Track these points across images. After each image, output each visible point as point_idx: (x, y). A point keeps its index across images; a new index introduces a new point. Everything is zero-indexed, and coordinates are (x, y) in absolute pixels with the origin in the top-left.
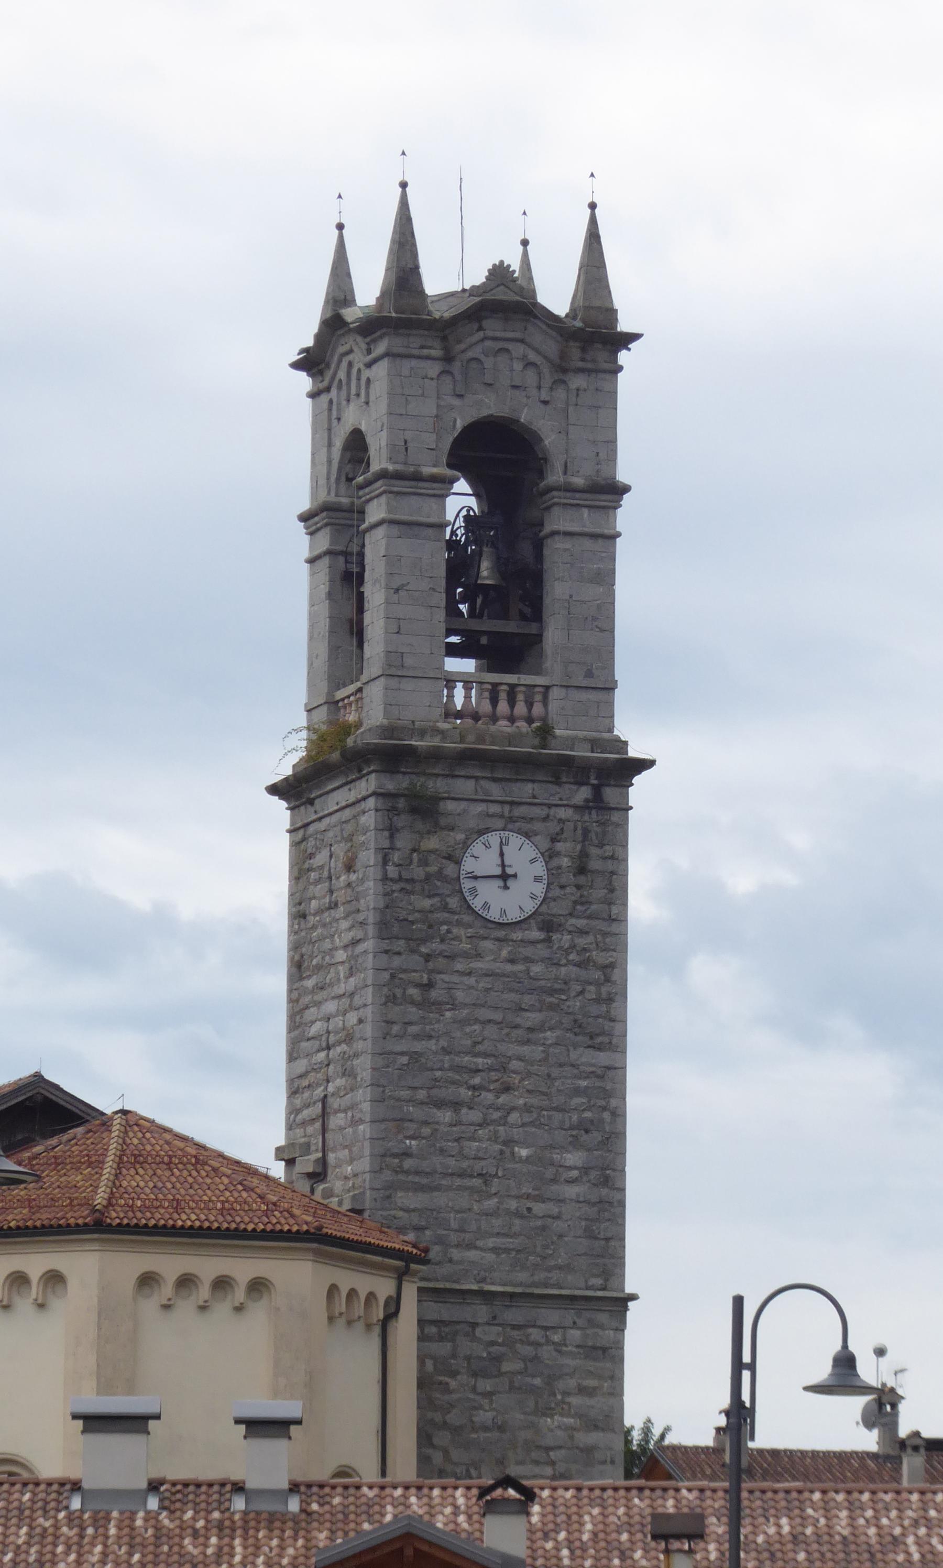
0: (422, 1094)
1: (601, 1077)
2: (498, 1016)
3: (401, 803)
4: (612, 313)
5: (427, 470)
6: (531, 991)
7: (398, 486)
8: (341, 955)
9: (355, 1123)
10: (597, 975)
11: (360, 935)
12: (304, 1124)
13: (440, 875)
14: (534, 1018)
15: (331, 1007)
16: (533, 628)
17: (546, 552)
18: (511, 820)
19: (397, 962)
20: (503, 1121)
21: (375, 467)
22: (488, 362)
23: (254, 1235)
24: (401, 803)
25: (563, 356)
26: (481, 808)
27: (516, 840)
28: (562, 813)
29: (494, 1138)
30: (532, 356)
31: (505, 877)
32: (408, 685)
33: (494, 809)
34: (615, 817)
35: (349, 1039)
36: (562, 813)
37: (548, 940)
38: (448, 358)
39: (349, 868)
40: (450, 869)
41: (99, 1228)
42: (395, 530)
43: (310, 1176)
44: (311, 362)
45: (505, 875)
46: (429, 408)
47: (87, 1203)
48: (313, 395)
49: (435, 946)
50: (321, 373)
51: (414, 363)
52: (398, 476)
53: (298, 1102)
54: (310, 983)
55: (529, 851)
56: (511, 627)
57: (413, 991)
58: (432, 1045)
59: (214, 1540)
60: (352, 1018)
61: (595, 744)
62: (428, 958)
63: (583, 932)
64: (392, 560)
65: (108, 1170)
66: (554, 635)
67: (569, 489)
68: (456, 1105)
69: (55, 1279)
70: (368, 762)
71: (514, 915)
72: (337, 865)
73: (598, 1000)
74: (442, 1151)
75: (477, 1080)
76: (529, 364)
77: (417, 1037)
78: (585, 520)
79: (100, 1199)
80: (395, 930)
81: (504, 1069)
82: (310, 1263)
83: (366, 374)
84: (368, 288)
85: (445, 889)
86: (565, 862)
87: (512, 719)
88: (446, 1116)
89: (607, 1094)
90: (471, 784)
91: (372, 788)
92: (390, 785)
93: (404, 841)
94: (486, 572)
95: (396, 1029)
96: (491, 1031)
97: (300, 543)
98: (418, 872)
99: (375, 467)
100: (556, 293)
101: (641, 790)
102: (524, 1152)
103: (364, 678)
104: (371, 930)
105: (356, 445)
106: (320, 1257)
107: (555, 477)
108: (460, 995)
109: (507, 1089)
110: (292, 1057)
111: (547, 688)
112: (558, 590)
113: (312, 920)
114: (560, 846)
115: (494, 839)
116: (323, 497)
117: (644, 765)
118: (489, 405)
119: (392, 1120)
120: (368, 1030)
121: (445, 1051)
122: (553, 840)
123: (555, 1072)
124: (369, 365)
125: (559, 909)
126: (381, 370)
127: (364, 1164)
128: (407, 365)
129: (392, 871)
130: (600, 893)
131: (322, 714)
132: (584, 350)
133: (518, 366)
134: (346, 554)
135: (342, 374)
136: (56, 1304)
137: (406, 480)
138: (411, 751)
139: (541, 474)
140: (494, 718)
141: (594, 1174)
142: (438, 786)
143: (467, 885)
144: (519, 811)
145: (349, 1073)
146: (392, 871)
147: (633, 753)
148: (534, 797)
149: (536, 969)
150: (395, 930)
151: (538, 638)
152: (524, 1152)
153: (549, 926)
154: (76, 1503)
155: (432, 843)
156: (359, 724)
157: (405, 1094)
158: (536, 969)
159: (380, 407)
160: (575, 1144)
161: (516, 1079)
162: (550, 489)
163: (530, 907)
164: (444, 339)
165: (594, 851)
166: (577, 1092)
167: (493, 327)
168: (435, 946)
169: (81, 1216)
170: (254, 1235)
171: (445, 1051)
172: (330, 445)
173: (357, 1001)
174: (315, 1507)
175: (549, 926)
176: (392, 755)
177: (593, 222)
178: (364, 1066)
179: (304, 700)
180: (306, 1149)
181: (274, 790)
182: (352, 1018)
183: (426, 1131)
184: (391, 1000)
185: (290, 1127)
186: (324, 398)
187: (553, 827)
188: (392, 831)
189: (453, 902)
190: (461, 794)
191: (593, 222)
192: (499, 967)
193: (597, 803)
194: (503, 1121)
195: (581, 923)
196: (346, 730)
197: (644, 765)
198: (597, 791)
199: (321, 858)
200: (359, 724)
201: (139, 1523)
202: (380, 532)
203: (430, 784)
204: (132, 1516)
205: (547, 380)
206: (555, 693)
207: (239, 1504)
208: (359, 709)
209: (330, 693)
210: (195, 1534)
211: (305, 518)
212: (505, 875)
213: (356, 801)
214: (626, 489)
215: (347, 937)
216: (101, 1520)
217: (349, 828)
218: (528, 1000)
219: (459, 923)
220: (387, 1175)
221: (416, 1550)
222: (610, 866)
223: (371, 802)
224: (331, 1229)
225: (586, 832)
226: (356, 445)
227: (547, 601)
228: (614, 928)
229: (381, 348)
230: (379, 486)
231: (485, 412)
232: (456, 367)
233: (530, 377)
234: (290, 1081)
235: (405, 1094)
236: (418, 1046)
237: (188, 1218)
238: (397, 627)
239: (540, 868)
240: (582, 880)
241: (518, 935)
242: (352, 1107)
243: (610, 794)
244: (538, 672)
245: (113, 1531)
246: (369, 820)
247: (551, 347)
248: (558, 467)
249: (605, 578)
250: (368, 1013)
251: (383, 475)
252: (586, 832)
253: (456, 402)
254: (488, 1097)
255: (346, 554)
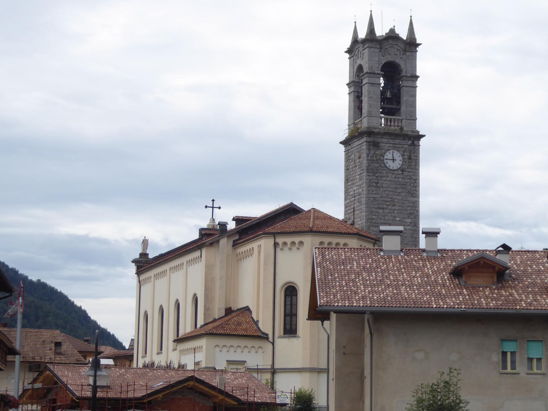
0: (376, 206)
1: (414, 203)
2: (392, 190)
3: (371, 144)
4: (415, 39)
5: (377, 72)
6: (399, 184)
7: (370, 75)
8: (358, 177)
9: (361, 212)
10: (413, 181)
11: (362, 172)
12: (349, 214)
13: (380, 159)
14: (400, 190)
15: (355, 188)
16: (398, 107)
17: (401, 90)
18: (395, 147)
19: (371, 178)
20: (393, 212)
21: (365, 71)
22: (389, 49)
23: (345, 234)
24: (371, 144)
25: (405, 48)
26: (388, 145)
27: (396, 152)
28: (406, 146)
29: (391, 216)
30: (398, 48)
31: (393, 160)
32: (372, 118)
33: (391, 145)
34: (417, 147)
35: (360, 194)
36: (406, 146)
37: (403, 174)
38: (381, 48)
39: (359, 158)
40: (382, 158)
41: (311, 232)
42: (370, 85)
43: (351, 224)
44: (350, 51)
45: (394, 159)
46: (377, 59)
47: (308, 226)
48: (349, 58)
49: (379, 174)
50: (352, 53)
51: (373, 49)
52: (370, 73)
53: (347, 209)
54: (350, 184)
55: (399, 154)
56: (393, 107)
57: (374, 184)
58: (378, 196)
59: (421, 262)
60: (360, 190)
61: (412, 131)
62: (377, 177)
63: (410, 172)
64: (369, 92)
65: (312, 220)
66: (403, 108)
67: (407, 76)
68: (383, 209)
69: (301, 243)
70: (364, 135)
71: (395, 168)
72: (356, 158)
73: (414, 187)
74: (380, 218)
75: (388, 203)
76: (398, 50)
77: (375, 194)
78: (410, 83)
79: (311, 225)
80: (370, 171)
81: (393, 201)
82: (356, 240)
83: (363, 52)
84: (362, 35)
85: (381, 162)
86: (406, 157)
87: (394, 126)
88: (381, 211)
89: (416, 207)
90: (386, 140)
91: (365, 140)
92: (369, 140)
93: (372, 152)
94: (388, 95)
95: (370, 192)
96: (391, 193)
97: (347, 90)
98: (375, 159)
99: (365, 71)
100: (403, 34)
101: (422, 141)
102: (398, 219)
103: (362, 117)
104: (365, 171)
105: (360, 68)
106: (359, 239)
107: (403, 74)
108: (384, 185)
109: (394, 205)
110: (345, 200)
111: (402, 119)
112: (404, 98)
113: (350, 170)
114: (405, 153)
115: (391, 151)
116: (352, 80)
117: (423, 136)
118: (389, 58)
119: (370, 212)
120: (365, 192)
121: (381, 197)
122: (404, 152)
123: (404, 202)
124: (363, 50)
125: (404, 167)
126: (366, 51)
127: (364, 221)
128: (372, 49)
129: (369, 158)
130: (414, 164)
131: (352, 126)
132: (410, 47)
133: (396, 50)
134: (358, 92)
135: (356, 53)
136: (302, 248)
137: (372, 74)
138: (374, 132)
139: (400, 74)
140: (391, 126)
141: (413, 224)
142: (380, 140)
143: (385, 161)
144: (396, 146)
145: (360, 202)
146: (369, 158)
147: (420, 134)
148: (78, 361)
149: (400, 180)
150: (370, 171)
151: (399, 109)
152: (398, 219)
153: (403, 171)
154: (382, 254)
155: (378, 152)
156: (361, 127)
157: (373, 206)
158: (400, 180)
159: (366, 58)
160: (409, 217)
161: (396, 203)
162: (402, 77)
163: (399, 166)
164: (380, 44)
165: (412, 155)
166: (409, 206)
167: (390, 42)
168: (379, 174)
169: (307, 229)
170: (345, 234)
171: (381, 197)
172: (354, 68)
173: (362, 186)
174: (445, 255)
175: (403, 171)
176: (369, 133)
177: (411, 20)
178: (364, 200)
179: (348, 123)
180: (350, 219)
181: (341, 143)
182: (360, 190)
183: (377, 214)
184: (369, 186)
185: (345, 215)
186: (352, 59)
187: (404, 149)
188: (369, 150)
189: (382, 165)
190: (384, 142)
191: (411, 20)
192: (392, 179)
193: (413, 144)
194: (393, 212)
195: (410, 170)
196: (358, 129)
197: (423, 136)
198: (413, 142)
199: (353, 156)
200: (361, 127)
201: (400, 258)
202: (366, 85)
203: (377, 140)
204: (398, 257)
205: (402, 53)
206: (404, 121)
207: (425, 254)
208: (361, 124)
209: (354, 121)
210: (416, 261)
211: (347, 85)
212: (394, 159)
213: (362, 144)
214: (419, 77)
215: (359, 173)
216: (390, 258)
217: (359, 150)
218: (398, 186)
219: (384, 170)
220: (369, 224)
221: (484, 262)
222: (416, 158)
223: (365, 143)
224: (360, 233)
225: (411, 150)
226: (360, 68)
227: (402, 101)
228: (417, 171)
229: (366, 46)
230: (366, 75)
231: (388, 60)
232: (383, 50)
233: (398, 53)
234: (345, 205)
235: (373, 206)
236: (375, 196)
237: (330, 230)
238: (370, 106)
239: (401, 158)
240: (410, 161)
241: (396, 172)
242: (361, 209)
243: (416, 142)
244: (400, 116)
245: (394, 260)
246: (364, 147)
247: (403, 46)
248: (404, 72)
249: (414, 96)
250: (365, 189)
251: (367, 73)
252: (411, 150)
253: (382, 58)
254: (390, 207)
255: (358, 92)
